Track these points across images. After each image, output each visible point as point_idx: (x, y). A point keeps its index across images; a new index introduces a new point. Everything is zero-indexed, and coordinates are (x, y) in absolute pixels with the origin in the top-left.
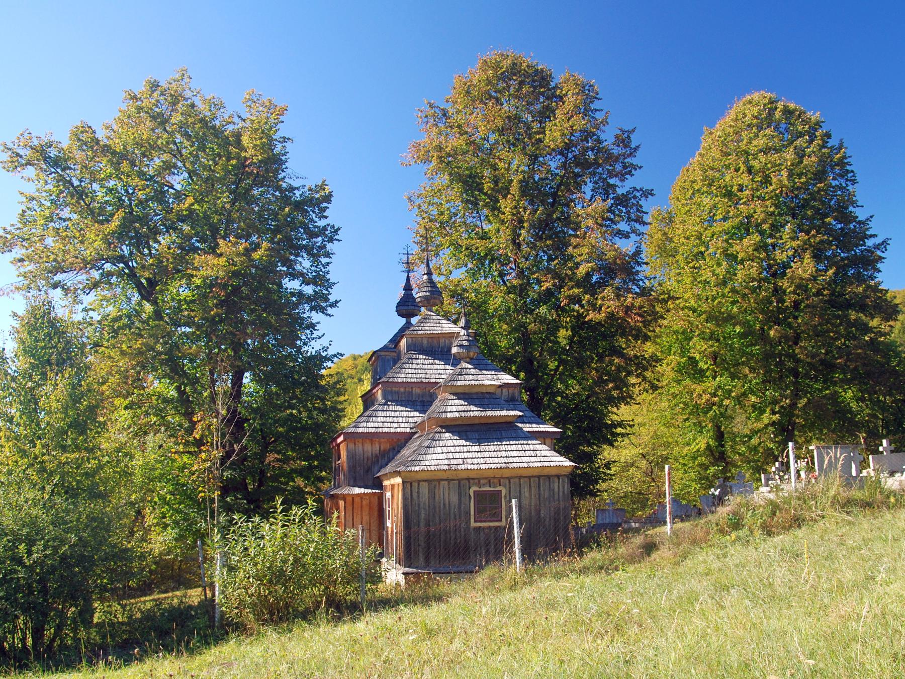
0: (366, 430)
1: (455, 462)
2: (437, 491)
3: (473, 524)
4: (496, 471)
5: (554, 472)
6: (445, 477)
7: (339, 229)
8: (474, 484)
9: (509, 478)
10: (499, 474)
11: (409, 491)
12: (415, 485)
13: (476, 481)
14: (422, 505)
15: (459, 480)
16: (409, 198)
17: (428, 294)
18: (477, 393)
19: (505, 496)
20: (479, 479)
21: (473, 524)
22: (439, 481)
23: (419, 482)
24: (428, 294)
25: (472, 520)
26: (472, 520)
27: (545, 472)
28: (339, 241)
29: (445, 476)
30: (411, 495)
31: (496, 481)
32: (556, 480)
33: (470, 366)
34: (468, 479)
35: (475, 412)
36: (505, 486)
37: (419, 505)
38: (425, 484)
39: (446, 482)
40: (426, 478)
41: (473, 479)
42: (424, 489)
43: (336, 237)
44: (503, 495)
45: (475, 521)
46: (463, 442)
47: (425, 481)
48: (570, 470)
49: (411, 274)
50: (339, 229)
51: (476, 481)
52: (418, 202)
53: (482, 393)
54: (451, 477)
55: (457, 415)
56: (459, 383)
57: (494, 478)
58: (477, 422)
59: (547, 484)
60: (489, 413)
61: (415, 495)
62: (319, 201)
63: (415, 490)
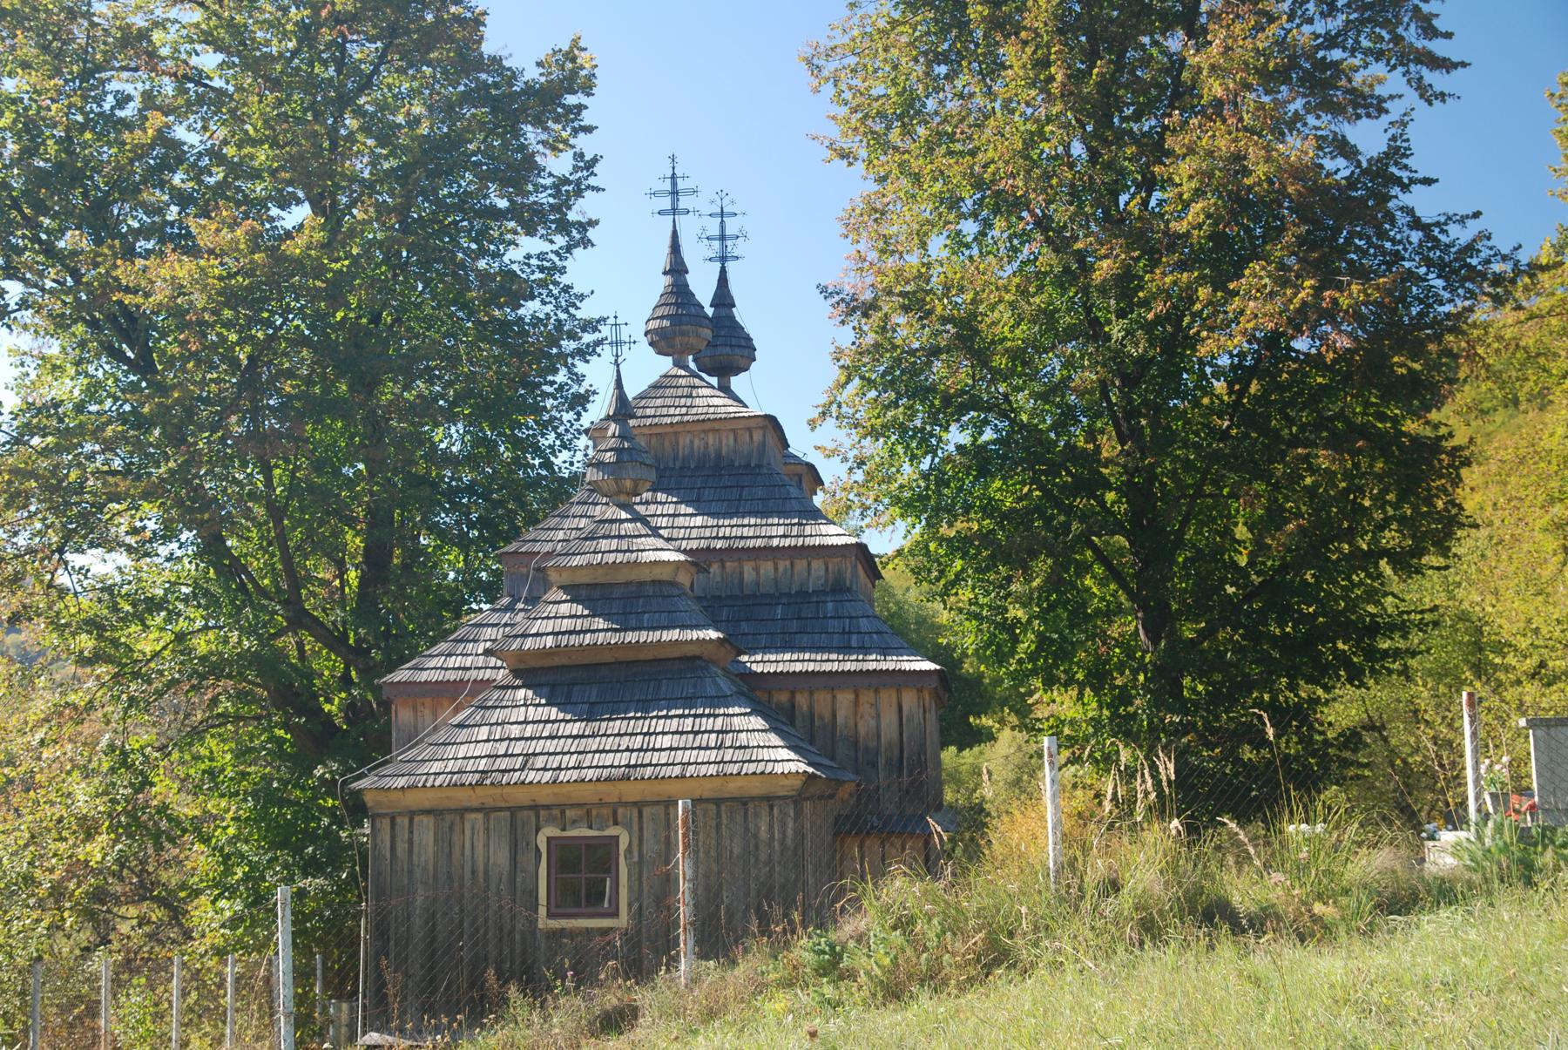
0: (435, 676)
1: (503, 764)
2: (455, 838)
3: (544, 922)
4: (601, 787)
5: (756, 788)
6: (475, 804)
7: (595, 160)
8: (551, 821)
9: (639, 805)
10: (613, 793)
11: (387, 838)
12: (403, 822)
13: (556, 812)
14: (418, 873)
15: (514, 810)
16: (809, 62)
17: (666, 323)
18: (627, 584)
19: (629, 850)
20: (562, 808)
21: (544, 922)
22: (463, 811)
23: (412, 814)
24: (666, 323)
25: (542, 911)
26: (542, 911)
27: (733, 787)
28: (597, 189)
29: (473, 799)
30: (393, 848)
31: (606, 812)
32: (764, 812)
33: (690, 510)
34: (535, 808)
35: (601, 633)
36: (628, 827)
37: (411, 872)
38: (427, 822)
39: (480, 816)
40: (427, 805)
41: (548, 807)
42: (426, 832)
43: (592, 181)
44: (623, 846)
45: (550, 915)
46: (554, 712)
47: (478, 810)
48: (797, 783)
49: (730, 265)
50: (595, 160)
51: (556, 812)
52: (830, 67)
53: (641, 584)
54: (490, 803)
55: (549, 641)
56: (576, 561)
57: (601, 804)
58: (608, 657)
59: (739, 819)
60: (631, 637)
61: (402, 847)
62: (559, 93)
63: (402, 835)
